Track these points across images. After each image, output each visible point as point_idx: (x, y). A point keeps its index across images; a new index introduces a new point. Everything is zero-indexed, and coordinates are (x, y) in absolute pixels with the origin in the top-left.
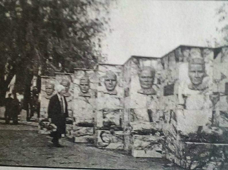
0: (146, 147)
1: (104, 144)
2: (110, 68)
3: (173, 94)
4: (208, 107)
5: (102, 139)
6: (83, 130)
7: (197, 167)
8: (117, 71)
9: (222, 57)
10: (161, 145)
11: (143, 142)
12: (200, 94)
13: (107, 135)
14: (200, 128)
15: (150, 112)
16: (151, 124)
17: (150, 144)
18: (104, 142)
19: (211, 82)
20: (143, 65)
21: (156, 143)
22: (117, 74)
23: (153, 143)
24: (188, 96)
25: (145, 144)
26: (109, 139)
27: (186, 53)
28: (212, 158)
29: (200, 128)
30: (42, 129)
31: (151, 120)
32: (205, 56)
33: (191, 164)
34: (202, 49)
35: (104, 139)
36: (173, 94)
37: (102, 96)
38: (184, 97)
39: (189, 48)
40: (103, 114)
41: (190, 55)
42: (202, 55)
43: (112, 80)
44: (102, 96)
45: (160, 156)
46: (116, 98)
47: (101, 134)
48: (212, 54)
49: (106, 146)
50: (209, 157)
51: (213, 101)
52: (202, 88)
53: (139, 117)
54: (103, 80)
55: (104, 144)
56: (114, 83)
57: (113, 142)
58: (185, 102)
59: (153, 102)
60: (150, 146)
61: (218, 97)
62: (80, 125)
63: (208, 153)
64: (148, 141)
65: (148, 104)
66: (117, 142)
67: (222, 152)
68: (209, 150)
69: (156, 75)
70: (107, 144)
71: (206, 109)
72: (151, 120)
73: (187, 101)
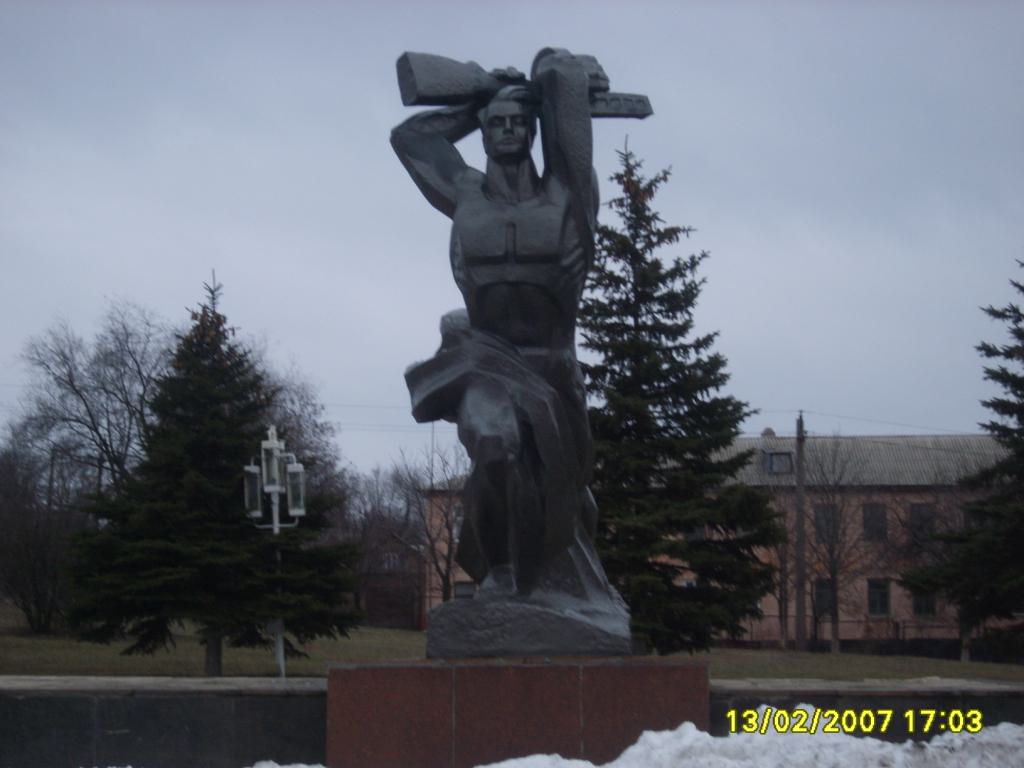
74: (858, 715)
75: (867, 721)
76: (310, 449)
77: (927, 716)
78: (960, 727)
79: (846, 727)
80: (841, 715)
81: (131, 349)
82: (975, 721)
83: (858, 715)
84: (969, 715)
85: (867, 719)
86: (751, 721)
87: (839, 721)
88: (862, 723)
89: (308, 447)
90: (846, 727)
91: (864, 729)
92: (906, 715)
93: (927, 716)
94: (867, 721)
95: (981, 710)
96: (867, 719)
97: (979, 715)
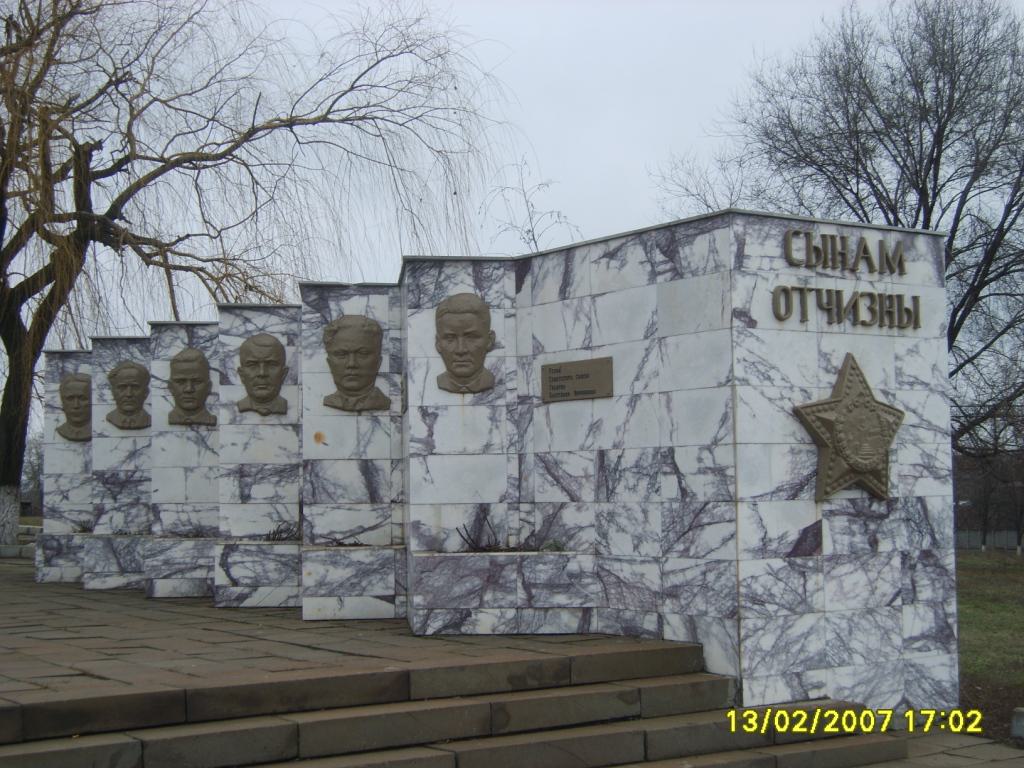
0: (341, 585)
1: (238, 590)
2: (260, 320)
3: (609, 395)
4: (506, 443)
5: (228, 574)
6: (182, 551)
7: (445, 627)
8: (283, 328)
9: (533, 287)
10: (391, 578)
11: (331, 569)
12: (475, 404)
13: (246, 559)
14: (483, 510)
15: (368, 469)
16: (374, 510)
17: (356, 576)
18: (235, 583)
19: (510, 365)
20: (341, 311)
21: (375, 571)
22: (283, 340)
23: (364, 572)
24: (439, 412)
25: (338, 574)
26: (253, 575)
27: (428, 280)
28: (488, 597)
29: (483, 510)
30: (48, 562)
31: (374, 497)
32: (490, 288)
33: (427, 617)
34: (477, 263)
35: (236, 572)
36: (609, 395)
37: (233, 422)
38: (424, 412)
39: (439, 263)
40: (241, 488)
41: (439, 286)
42: (479, 282)
43: (268, 363)
44: (233, 422)
45: (386, 610)
46: (284, 425)
47: (225, 556)
48: (509, 282)
49: (242, 597)
50: (479, 593)
51: (517, 423)
52: (482, 385)
53: (331, 489)
54: (236, 362)
55: (238, 590)
56: (274, 371)
57: (269, 584)
58: (431, 434)
59: (380, 435)
60: (355, 580)
61: (530, 412)
62: (176, 534)
63: (477, 581)
64: (348, 566)
65: (363, 441)
66: (280, 583)
67: (514, 576)
68: (477, 573)
69: (386, 343)
70: (247, 590)
71: (127, 445)
72: (374, 497)
73: (437, 428)
74: (858, 726)
75: (849, 721)
76: (189, 438)
77: (928, 716)
78: (952, 715)
79: (871, 715)
80: (841, 715)
81: (796, 126)
82: (751, 721)
83: (858, 726)
84: (969, 715)
85: (849, 723)
86: (751, 721)
87: (840, 720)
88: (776, 723)
89: (122, 218)
90: (871, 715)
91: (852, 713)
92: (906, 715)
93: (928, 716)
94: (849, 721)
95: (980, 710)
96: (849, 723)
97: (979, 716)
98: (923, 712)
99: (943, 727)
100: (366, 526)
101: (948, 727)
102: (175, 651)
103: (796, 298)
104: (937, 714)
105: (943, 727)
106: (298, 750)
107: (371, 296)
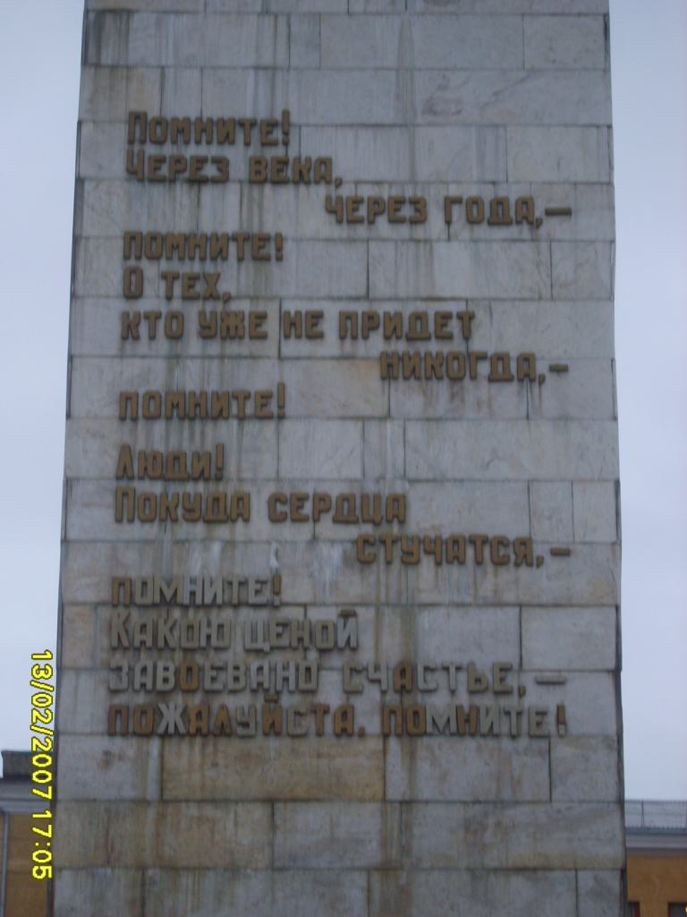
74: (38, 769)
75: (42, 777)
80: (47, 753)
83: (38, 769)
85: (44, 777)
87: (43, 752)
88: (44, 765)
91: (49, 763)
94: (42, 777)
96: (44, 777)
98: (50, 826)
99: (37, 844)
100: (481, 799)
101: (37, 849)
102: (554, 61)
103: (161, 643)
104: (49, 840)
105: (37, 844)
106: (102, 541)
107: (639, 825)
